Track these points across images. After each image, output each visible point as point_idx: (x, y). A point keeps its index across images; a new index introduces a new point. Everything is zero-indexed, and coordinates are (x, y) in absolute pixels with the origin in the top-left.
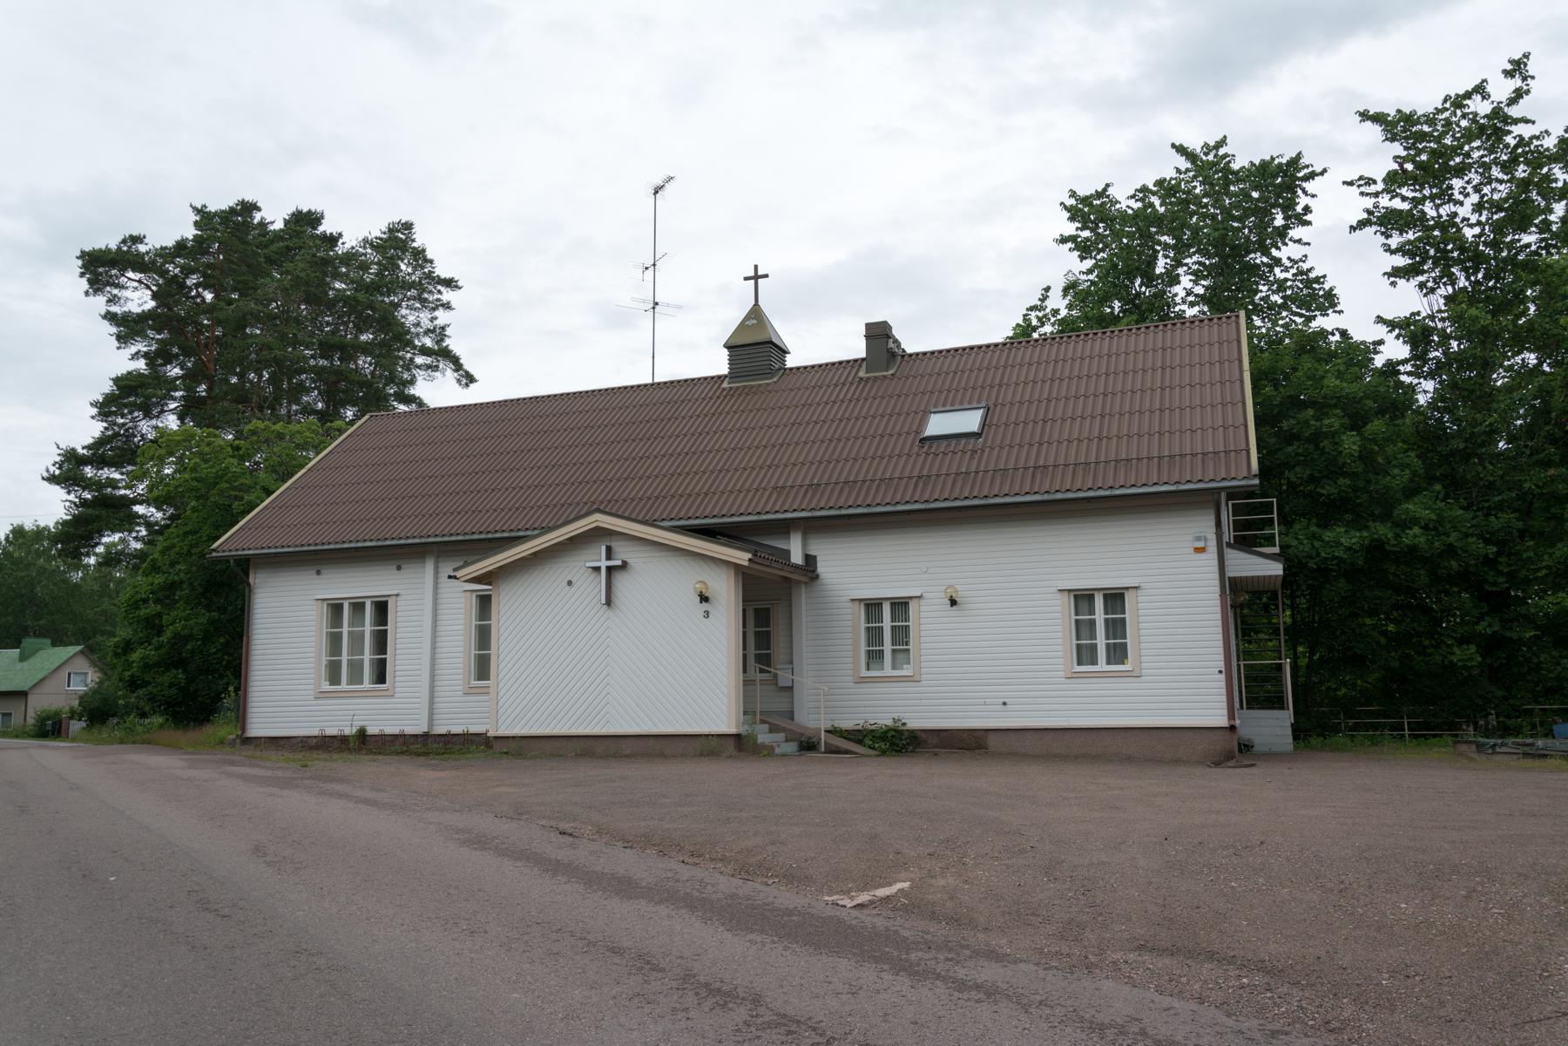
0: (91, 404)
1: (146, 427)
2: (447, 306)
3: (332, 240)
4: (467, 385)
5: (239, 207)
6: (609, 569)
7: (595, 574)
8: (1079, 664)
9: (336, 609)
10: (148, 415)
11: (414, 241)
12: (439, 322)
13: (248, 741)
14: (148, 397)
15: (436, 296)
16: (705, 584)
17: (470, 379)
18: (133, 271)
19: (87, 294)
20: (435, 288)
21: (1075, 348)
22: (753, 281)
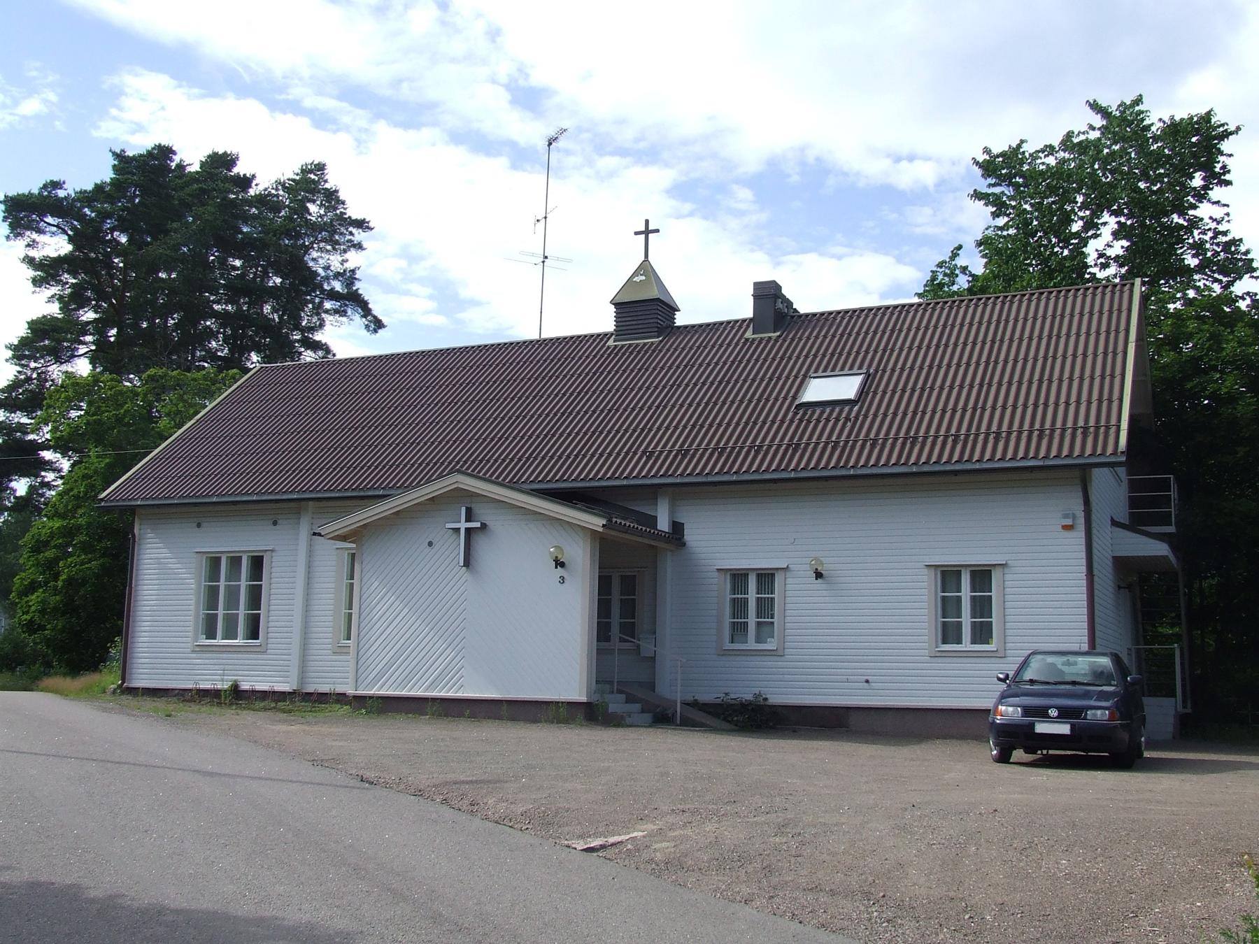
0: (6, 347)
1: (56, 372)
2: (359, 246)
3: (245, 182)
4: (375, 331)
5: (156, 152)
6: (468, 530)
7: (454, 536)
8: (944, 642)
9: (214, 562)
10: (59, 361)
11: (326, 181)
12: (350, 266)
13: (133, 691)
14: (59, 341)
15: (348, 237)
16: (562, 550)
17: (378, 325)
18: (52, 216)
19: (8, 238)
20: (347, 229)
21: (991, 309)
22: (643, 236)
